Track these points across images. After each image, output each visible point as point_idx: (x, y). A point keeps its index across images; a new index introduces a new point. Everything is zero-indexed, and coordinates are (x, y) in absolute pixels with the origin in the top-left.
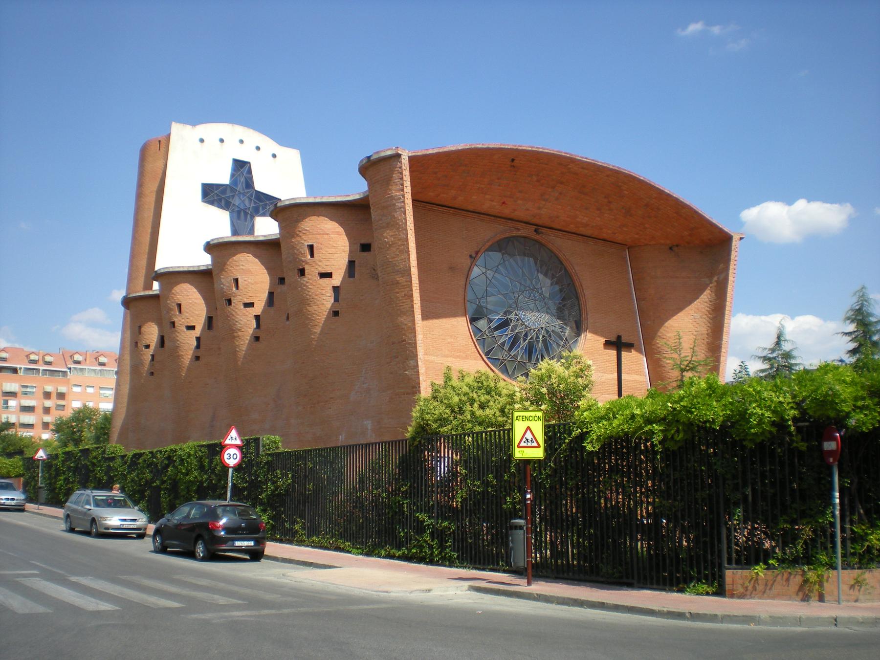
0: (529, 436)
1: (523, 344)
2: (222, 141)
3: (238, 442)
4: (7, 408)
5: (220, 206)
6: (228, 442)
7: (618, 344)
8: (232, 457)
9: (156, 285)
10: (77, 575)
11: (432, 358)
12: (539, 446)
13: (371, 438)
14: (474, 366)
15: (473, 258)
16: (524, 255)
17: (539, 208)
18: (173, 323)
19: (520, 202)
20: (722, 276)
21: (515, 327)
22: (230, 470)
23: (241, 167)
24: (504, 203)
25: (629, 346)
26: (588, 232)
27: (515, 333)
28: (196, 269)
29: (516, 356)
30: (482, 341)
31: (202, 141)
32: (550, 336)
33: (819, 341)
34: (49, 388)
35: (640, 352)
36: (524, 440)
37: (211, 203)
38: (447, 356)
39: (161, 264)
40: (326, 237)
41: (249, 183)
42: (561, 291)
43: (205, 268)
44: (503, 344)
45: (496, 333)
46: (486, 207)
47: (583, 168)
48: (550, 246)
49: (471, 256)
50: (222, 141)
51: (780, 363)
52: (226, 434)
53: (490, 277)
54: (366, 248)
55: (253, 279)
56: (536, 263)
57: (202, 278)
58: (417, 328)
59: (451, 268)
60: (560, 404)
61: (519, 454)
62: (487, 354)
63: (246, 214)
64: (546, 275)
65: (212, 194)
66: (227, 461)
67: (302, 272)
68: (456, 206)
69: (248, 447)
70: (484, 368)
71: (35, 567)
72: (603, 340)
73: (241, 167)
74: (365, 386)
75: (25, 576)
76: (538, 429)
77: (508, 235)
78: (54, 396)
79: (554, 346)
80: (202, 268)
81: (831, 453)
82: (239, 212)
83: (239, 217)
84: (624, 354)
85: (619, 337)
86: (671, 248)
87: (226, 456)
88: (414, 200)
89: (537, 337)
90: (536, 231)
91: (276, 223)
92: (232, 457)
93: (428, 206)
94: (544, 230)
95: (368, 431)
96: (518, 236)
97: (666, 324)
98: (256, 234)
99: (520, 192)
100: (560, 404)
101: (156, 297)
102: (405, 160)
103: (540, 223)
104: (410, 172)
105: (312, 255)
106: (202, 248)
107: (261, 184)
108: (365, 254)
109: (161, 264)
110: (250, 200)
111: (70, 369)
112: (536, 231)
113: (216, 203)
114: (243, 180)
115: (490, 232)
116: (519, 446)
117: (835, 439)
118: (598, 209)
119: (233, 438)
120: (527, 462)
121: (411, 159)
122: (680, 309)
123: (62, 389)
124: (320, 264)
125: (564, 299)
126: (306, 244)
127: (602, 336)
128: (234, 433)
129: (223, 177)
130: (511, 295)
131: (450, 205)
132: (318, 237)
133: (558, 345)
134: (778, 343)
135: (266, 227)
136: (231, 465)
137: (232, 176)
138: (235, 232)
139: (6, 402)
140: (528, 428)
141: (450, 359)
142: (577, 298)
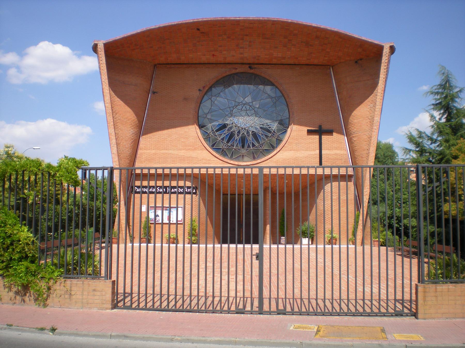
17: (241, 54)
26: (291, 62)
35: (341, 133)
45: (217, 133)
46: (204, 59)
47: (252, 23)
48: (263, 75)
49: (200, 90)
51: (416, 140)
72: (305, 129)
85: (320, 127)
86: (356, 62)
94: (256, 66)
96: (237, 73)
97: (353, 114)
103: (251, 62)
106: (396, 50)
112: (250, 68)
115: (213, 74)
122: (361, 103)
127: (306, 125)
130: (228, 109)
131: (178, 63)
141: (182, 151)
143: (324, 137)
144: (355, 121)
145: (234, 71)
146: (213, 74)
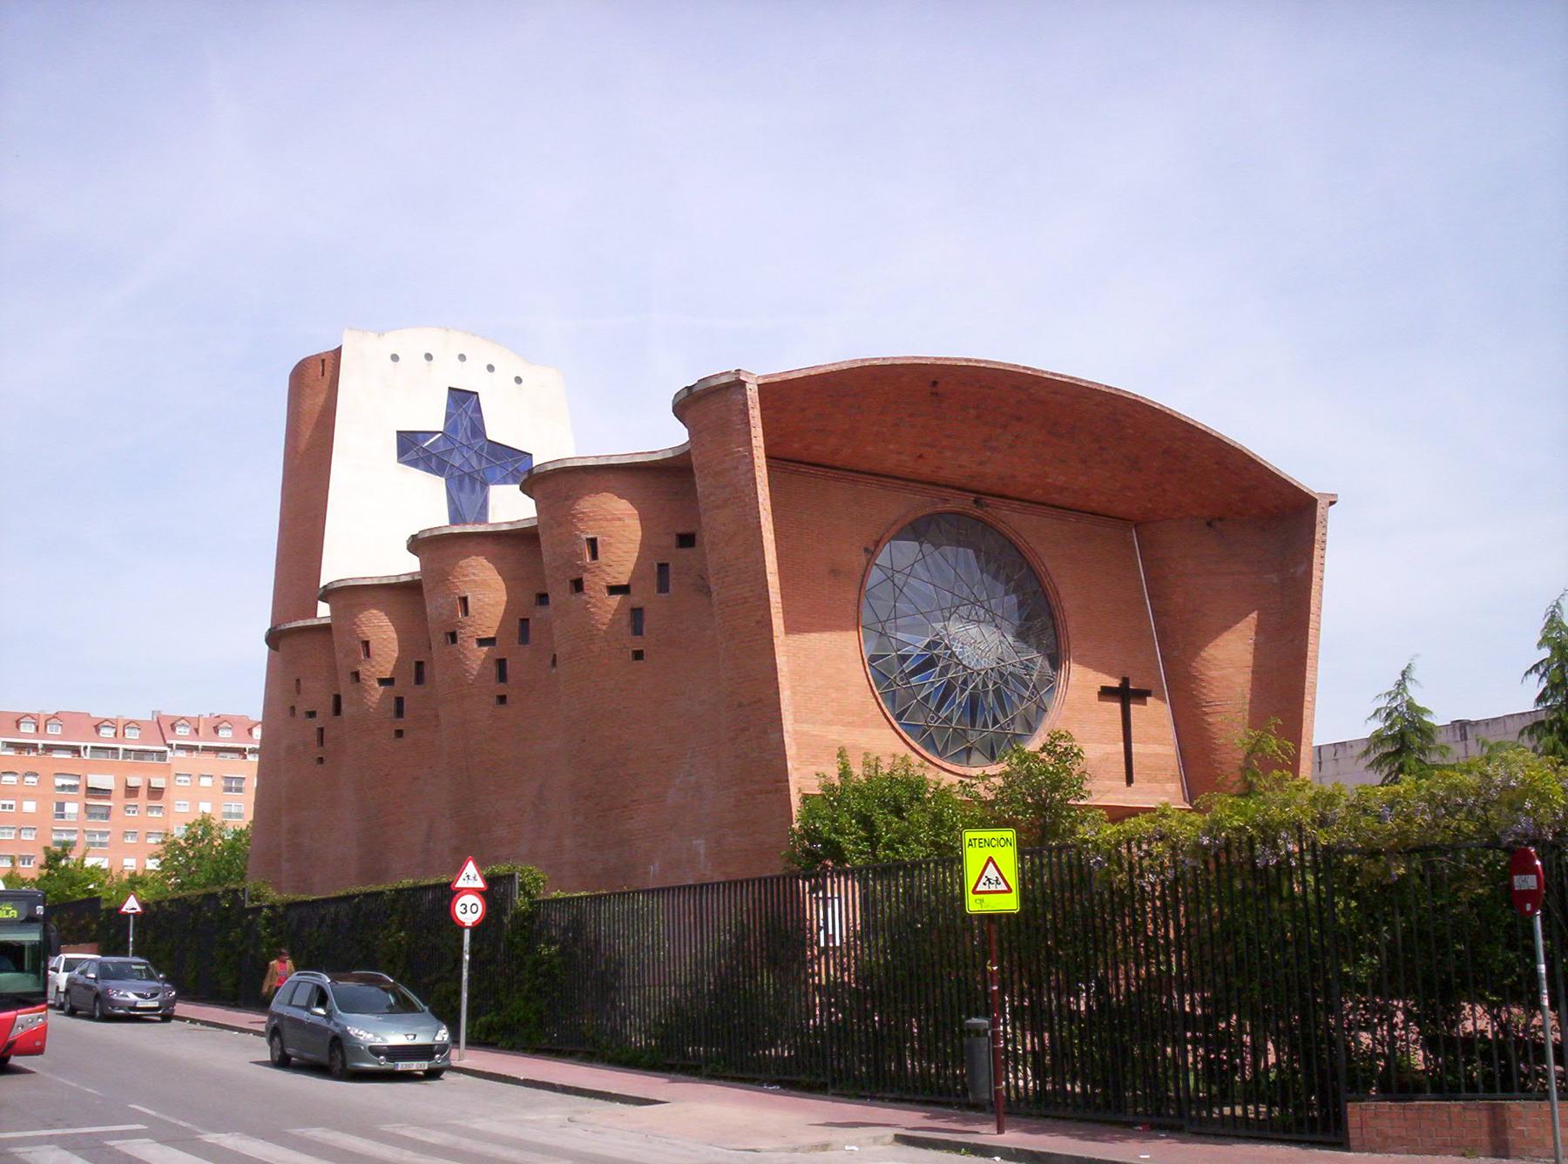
0: (991, 872)
1: (961, 698)
2: (429, 357)
3: (480, 884)
4: (63, 816)
5: (429, 470)
6: (460, 884)
7: (1125, 695)
8: (469, 911)
9: (324, 610)
10: (216, 1129)
11: (806, 727)
12: (1009, 891)
13: (707, 871)
14: (882, 745)
15: (871, 552)
16: (959, 545)
18: (356, 675)
19: (949, 454)
20: (1302, 568)
21: (946, 669)
22: (467, 933)
23: (463, 401)
24: (921, 456)
25: (1142, 695)
27: (945, 679)
28: (393, 581)
29: (948, 719)
30: (891, 697)
31: (395, 358)
32: (1006, 682)
33: (1485, 685)
34: (134, 781)
36: (984, 879)
37: (413, 463)
38: (829, 723)
39: (333, 570)
40: (618, 523)
41: (478, 428)
42: (1021, 605)
43: (408, 579)
44: (926, 699)
45: (914, 680)
49: (866, 550)
50: (429, 357)
52: (459, 869)
53: (900, 584)
54: (686, 540)
55: (487, 592)
56: (977, 557)
57: (401, 594)
58: (780, 679)
59: (834, 572)
60: (1040, 816)
61: (974, 905)
62: (899, 717)
63: (473, 480)
64: (995, 577)
65: (411, 447)
66: (461, 917)
67: (578, 585)
68: (838, 464)
69: (494, 892)
70: (903, 750)
71: (138, 1117)
73: (463, 401)
74: (693, 779)
75: (122, 1135)
76: (1007, 859)
77: (927, 511)
78: (143, 793)
79: (1015, 698)
80: (403, 579)
81: (1528, 895)
82: (461, 481)
83: (461, 487)
84: (1134, 708)
87: (458, 909)
88: (768, 457)
89: (985, 685)
90: (976, 502)
91: (532, 502)
92: (469, 911)
93: (791, 466)
94: (989, 500)
95: (698, 857)
98: (491, 519)
99: (949, 436)
100: (1040, 816)
101: (326, 629)
102: (752, 392)
104: (762, 410)
105: (594, 556)
106: (405, 545)
107: (496, 431)
108: (685, 551)
109: (333, 570)
110: (480, 456)
111: (170, 746)
113: (421, 463)
114: (466, 422)
115: (915, 503)
116: (975, 892)
117: (1534, 870)
118: (1084, 461)
119: (470, 876)
120: (991, 919)
121: (764, 389)
122: (1227, 627)
123: (158, 782)
124: (608, 570)
125: (1028, 619)
126: (584, 536)
128: (471, 868)
129: (431, 417)
132: (605, 524)
133: (1021, 698)
134: (1401, 685)
135: (510, 506)
136: (468, 923)
137: (448, 416)
138: (456, 516)
139: (61, 806)
140: (990, 859)
142: (1052, 616)
143: (1134, 708)
144: (1212, 673)
145: (940, 507)
146: (915, 503)
